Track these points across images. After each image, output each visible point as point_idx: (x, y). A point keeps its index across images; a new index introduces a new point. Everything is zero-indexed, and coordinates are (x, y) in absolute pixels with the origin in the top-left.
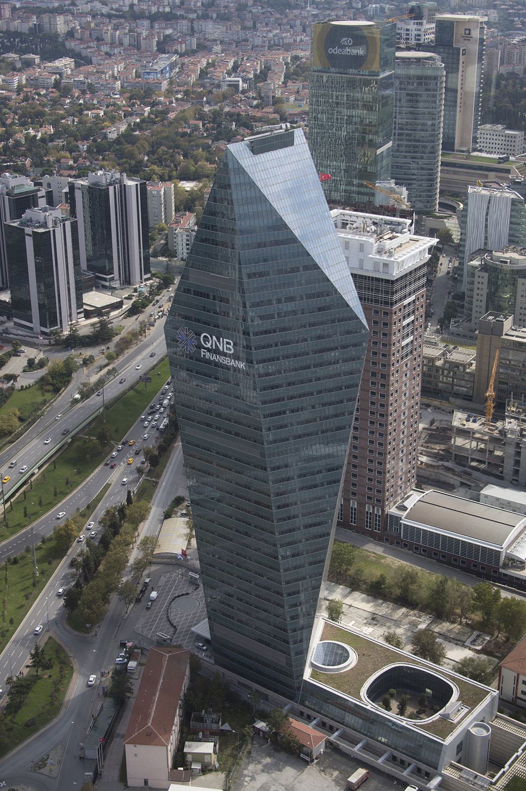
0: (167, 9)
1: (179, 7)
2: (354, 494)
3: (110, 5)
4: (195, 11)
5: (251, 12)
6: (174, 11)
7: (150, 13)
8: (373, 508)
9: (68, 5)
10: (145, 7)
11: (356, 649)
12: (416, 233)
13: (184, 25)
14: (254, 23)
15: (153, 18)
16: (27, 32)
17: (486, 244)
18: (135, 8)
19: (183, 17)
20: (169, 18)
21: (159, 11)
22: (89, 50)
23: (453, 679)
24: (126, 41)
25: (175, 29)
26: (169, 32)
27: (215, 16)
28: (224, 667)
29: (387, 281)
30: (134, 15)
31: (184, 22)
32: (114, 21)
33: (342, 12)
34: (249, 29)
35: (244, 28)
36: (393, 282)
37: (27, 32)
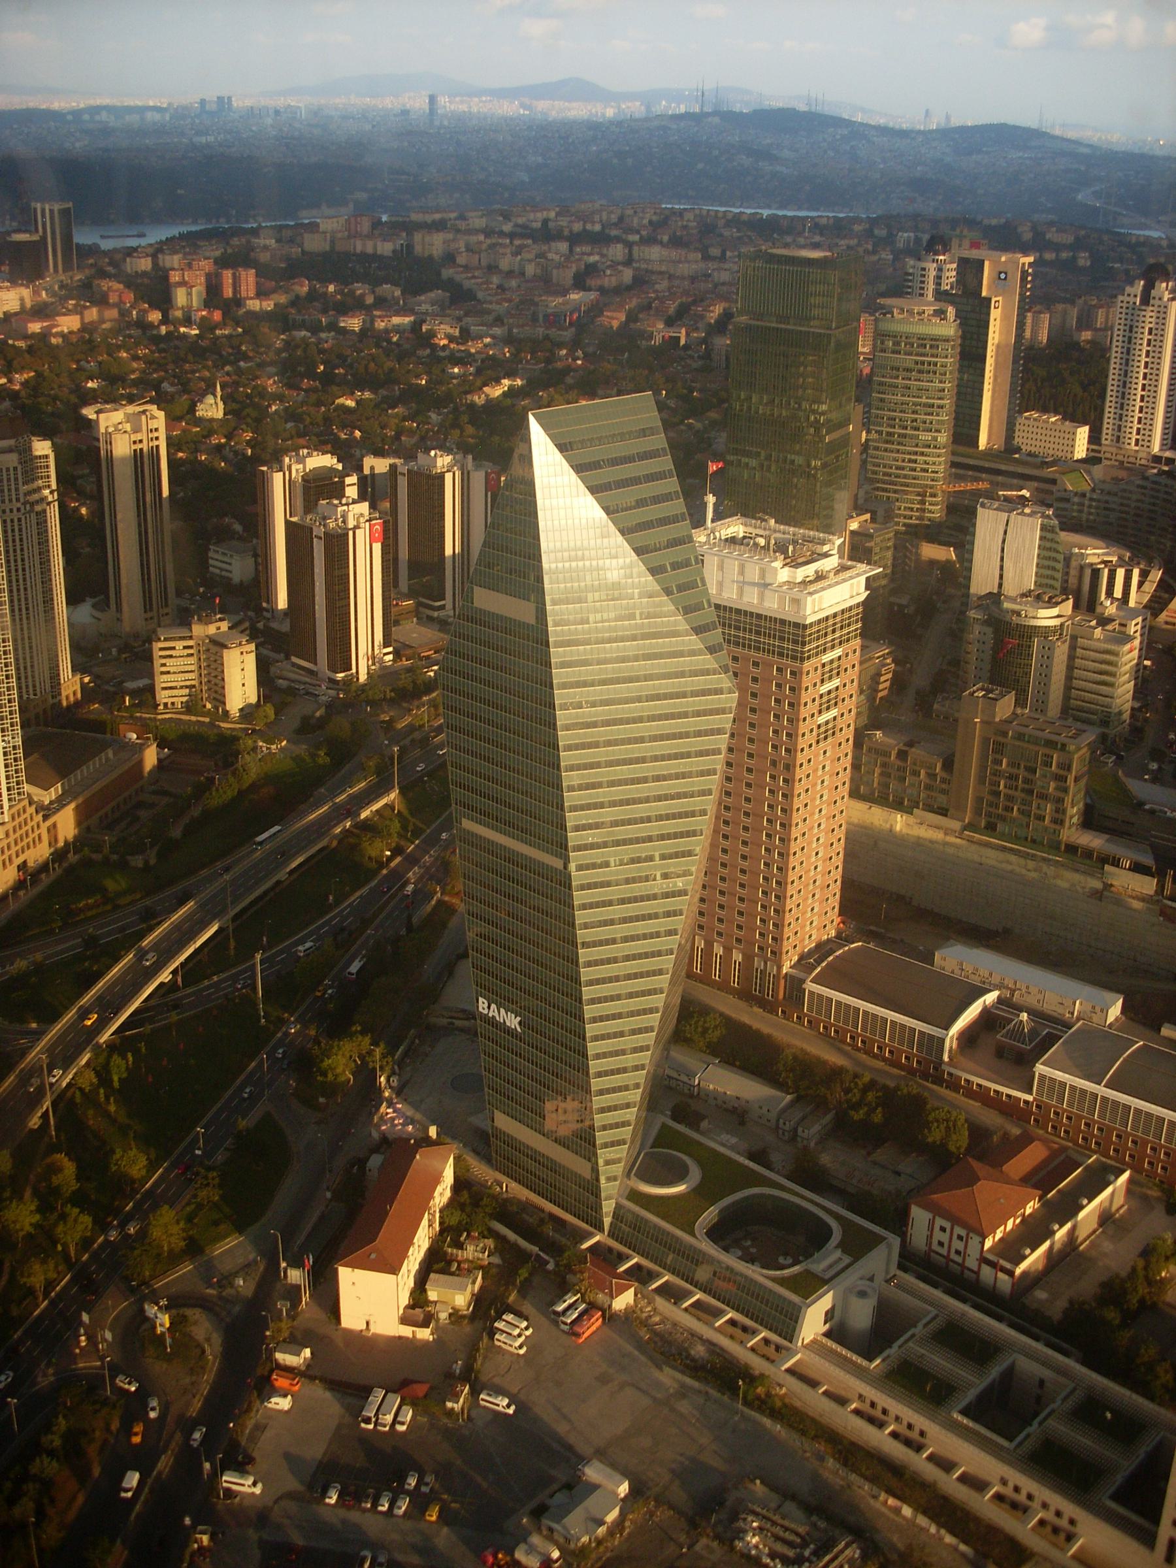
0: (598, 228)
1: (615, 225)
2: (720, 934)
3: (514, 219)
4: (638, 232)
5: (721, 235)
6: (607, 231)
7: (571, 231)
8: (766, 963)
9: (456, 219)
10: (564, 224)
11: (699, 1161)
12: (851, 558)
13: (617, 251)
14: (724, 253)
15: (574, 239)
16: (391, 254)
17: (1000, 585)
18: (551, 225)
19: (618, 240)
20: (601, 239)
21: (585, 230)
22: (473, 281)
23: (837, 1217)
24: (530, 270)
25: (603, 256)
26: (593, 259)
27: (666, 238)
28: (924, 1281)
29: (797, 625)
30: (546, 234)
31: (620, 246)
32: (517, 242)
33: (856, 241)
34: (713, 259)
35: (706, 257)
36: (805, 627)
37: (391, 254)
